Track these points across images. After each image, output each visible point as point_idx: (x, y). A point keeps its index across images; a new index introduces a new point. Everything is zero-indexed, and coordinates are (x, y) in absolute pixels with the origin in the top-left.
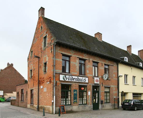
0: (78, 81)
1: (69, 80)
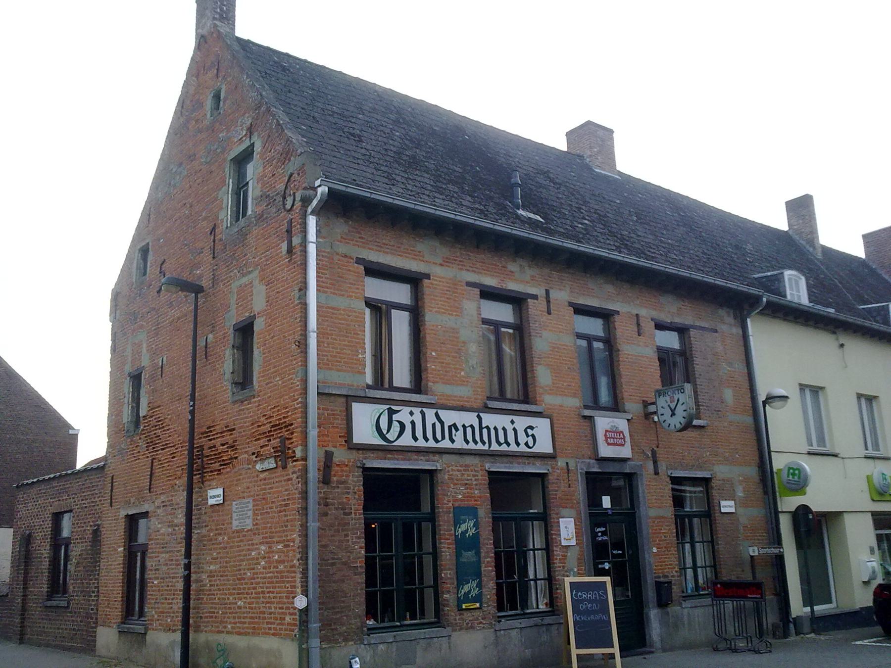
0: (480, 446)
1: (467, 442)
